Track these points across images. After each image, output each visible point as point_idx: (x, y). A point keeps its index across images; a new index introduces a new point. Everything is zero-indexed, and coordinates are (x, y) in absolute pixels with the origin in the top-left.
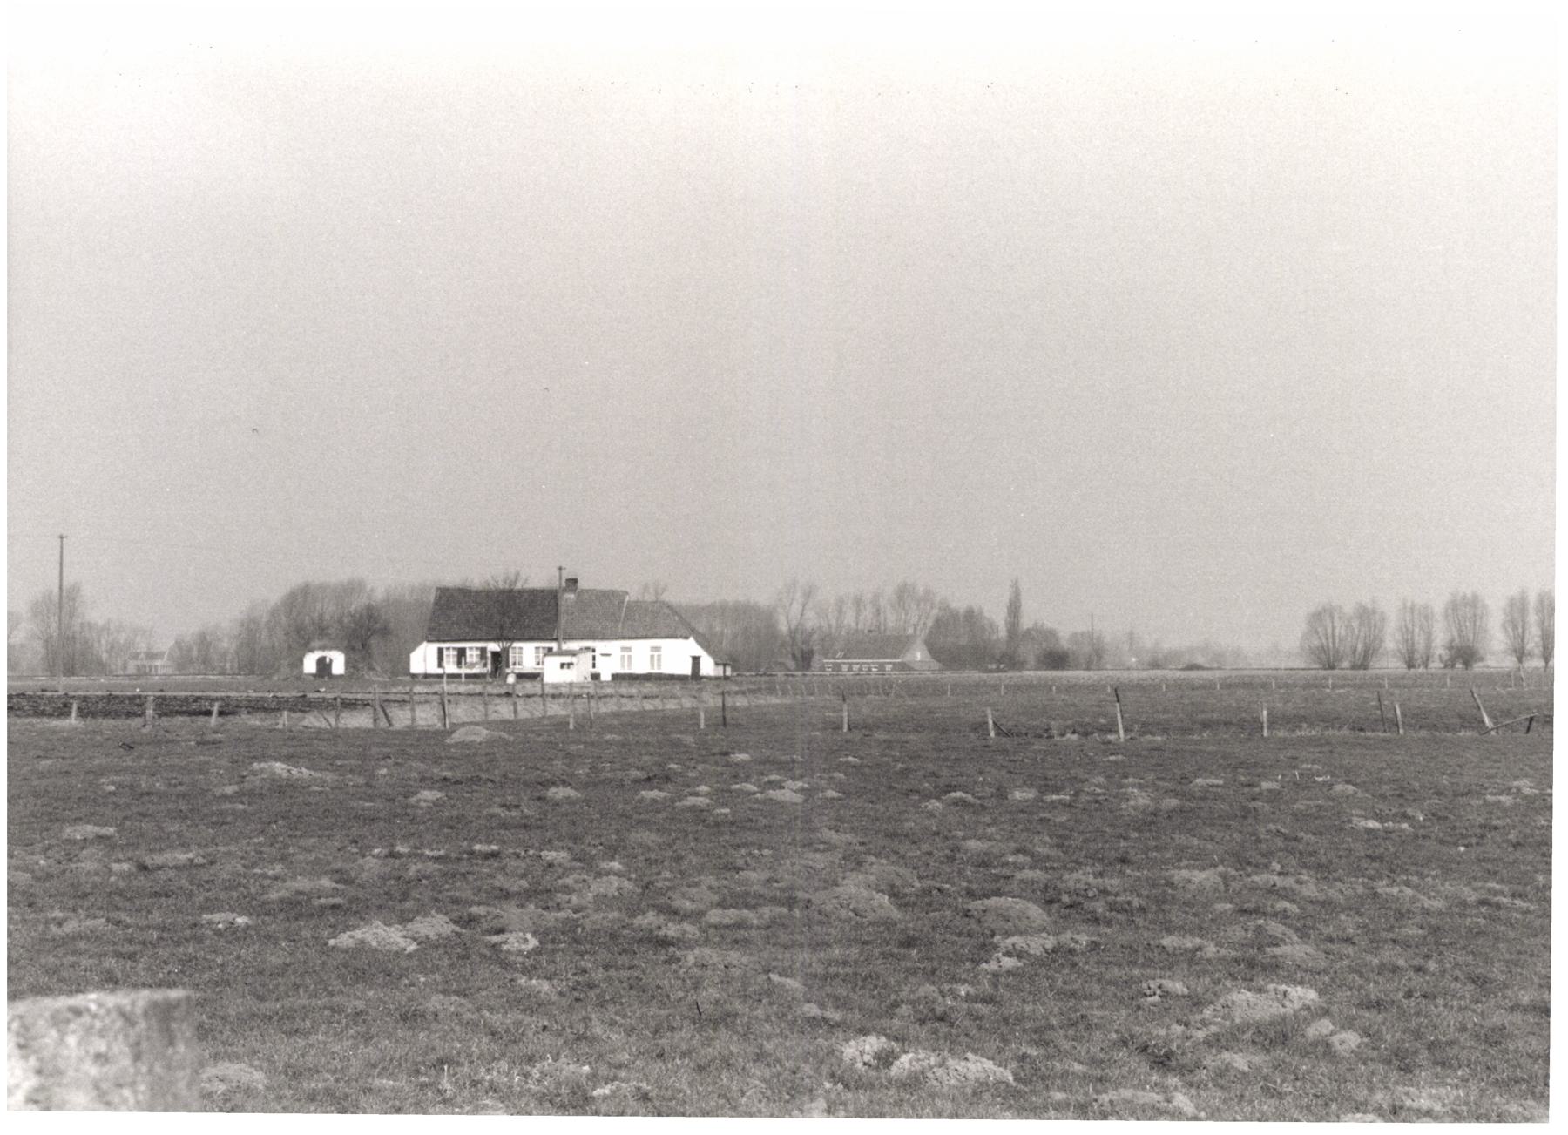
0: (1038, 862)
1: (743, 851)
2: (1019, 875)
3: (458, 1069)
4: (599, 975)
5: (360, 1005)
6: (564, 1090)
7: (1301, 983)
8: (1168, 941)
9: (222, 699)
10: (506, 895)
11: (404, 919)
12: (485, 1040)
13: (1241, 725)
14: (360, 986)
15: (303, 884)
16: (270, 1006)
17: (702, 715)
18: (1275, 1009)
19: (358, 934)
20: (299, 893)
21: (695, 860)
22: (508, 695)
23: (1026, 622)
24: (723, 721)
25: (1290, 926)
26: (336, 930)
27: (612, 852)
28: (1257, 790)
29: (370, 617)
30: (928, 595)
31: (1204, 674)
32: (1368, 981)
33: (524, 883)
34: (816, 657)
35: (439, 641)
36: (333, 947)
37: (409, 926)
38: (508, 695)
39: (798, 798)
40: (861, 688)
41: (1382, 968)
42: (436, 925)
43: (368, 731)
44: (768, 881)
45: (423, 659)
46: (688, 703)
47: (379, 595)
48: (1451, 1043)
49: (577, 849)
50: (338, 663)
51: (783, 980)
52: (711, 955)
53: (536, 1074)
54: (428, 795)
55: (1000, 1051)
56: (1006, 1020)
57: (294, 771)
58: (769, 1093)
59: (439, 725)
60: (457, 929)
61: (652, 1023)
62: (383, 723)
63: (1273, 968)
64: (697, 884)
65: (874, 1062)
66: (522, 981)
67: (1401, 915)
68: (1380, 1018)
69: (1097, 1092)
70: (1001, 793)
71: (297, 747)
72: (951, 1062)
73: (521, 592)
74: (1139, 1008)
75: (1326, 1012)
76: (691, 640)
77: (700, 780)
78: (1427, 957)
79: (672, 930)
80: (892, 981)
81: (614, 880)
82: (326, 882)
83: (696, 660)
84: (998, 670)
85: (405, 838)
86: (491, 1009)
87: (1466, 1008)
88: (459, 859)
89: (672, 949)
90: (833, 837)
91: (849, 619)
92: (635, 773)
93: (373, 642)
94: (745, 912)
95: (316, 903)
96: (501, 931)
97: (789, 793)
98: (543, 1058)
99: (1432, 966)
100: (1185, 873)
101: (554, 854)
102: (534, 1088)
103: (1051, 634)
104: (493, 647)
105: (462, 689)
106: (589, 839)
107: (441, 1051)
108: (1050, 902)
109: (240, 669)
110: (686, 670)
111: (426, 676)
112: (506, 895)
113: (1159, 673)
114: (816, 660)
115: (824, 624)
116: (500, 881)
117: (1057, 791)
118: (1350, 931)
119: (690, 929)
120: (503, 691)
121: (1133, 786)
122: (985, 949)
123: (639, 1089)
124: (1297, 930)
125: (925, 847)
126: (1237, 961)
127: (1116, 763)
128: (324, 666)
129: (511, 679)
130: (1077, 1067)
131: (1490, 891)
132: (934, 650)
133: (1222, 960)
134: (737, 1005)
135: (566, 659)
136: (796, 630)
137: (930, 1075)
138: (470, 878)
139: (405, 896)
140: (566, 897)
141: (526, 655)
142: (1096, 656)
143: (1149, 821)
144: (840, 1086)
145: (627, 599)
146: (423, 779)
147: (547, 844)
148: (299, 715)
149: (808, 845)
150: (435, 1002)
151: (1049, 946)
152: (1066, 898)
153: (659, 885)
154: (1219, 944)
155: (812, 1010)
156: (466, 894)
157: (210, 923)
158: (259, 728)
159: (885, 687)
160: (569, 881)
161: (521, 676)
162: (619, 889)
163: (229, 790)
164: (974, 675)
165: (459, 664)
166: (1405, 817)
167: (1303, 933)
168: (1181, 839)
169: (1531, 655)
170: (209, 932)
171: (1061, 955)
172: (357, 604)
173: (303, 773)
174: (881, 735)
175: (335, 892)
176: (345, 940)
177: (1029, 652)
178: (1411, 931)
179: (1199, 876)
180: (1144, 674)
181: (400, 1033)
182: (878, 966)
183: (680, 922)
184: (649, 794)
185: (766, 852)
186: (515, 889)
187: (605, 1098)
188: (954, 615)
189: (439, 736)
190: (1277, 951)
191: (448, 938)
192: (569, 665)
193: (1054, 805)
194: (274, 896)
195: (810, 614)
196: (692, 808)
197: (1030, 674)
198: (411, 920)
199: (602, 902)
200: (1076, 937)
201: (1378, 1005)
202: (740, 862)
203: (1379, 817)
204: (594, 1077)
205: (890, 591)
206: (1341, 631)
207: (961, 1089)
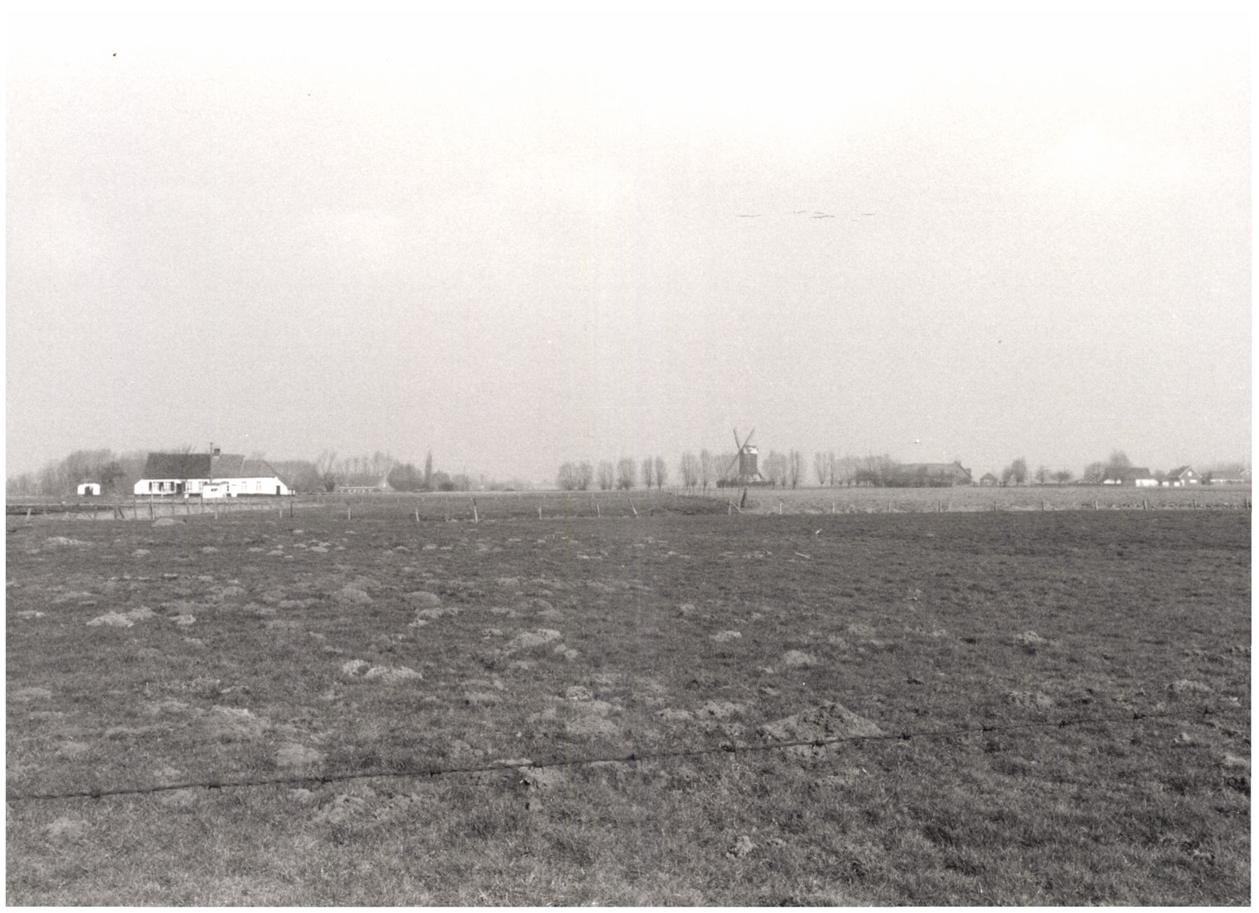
0: (436, 575)
1: (298, 574)
2: (428, 582)
3: (154, 684)
4: (226, 635)
5: (103, 655)
6: (207, 691)
7: (553, 628)
8: (495, 610)
9: (33, 507)
10: (179, 597)
11: (127, 610)
12: (168, 670)
13: (530, 515)
14: (103, 646)
15: (74, 594)
16: (53, 659)
17: (281, 513)
18: (541, 641)
19: (102, 618)
20: (71, 599)
21: (275, 578)
22: (184, 504)
23: (435, 470)
24: (291, 515)
25: (549, 601)
26: (90, 616)
27: (234, 576)
28: (535, 543)
29: (113, 468)
30: (389, 459)
31: (514, 493)
32: (582, 626)
33: (189, 591)
34: (336, 486)
35: (149, 478)
36: (90, 626)
37: (130, 613)
38: (184, 504)
39: (326, 550)
40: (358, 499)
41: (588, 620)
42: (144, 613)
43: (111, 521)
44: (310, 587)
45: (141, 487)
46: (274, 507)
47: (118, 457)
48: (617, 653)
49: (217, 575)
50: (96, 489)
51: (315, 635)
52: (280, 623)
53: (194, 685)
54: (142, 552)
55: (417, 665)
56: (420, 650)
57: (71, 541)
58: (308, 688)
59: (149, 518)
60: (155, 614)
61: (252, 658)
62: (119, 517)
63: (540, 621)
64: (276, 589)
65: (358, 673)
66: (188, 640)
67: (598, 595)
68: (586, 643)
69: (461, 681)
70: (421, 546)
71: (71, 529)
72: (394, 671)
73: (191, 456)
74: (480, 642)
75: (563, 641)
76: (276, 478)
77: (279, 543)
78: (607, 614)
79: (263, 611)
80: (367, 634)
81: (235, 587)
82: (86, 594)
83: (278, 488)
84: (421, 492)
85: (130, 572)
86: (172, 654)
87: (623, 637)
88: (156, 581)
89: (262, 621)
90: (342, 567)
91: (352, 469)
92: (247, 540)
93: (115, 480)
94: (298, 602)
95: (80, 603)
96: (177, 614)
97: (321, 548)
98: (196, 677)
99: (609, 618)
100: (503, 579)
101: (205, 577)
102: (191, 690)
103: (446, 476)
104: (177, 481)
105: (161, 501)
106: (223, 570)
107: (145, 675)
108: (442, 593)
109: (43, 492)
110: (274, 492)
111: (143, 495)
112: (179, 597)
113: (494, 493)
114: (337, 487)
115: (340, 471)
116: (177, 590)
117: (445, 545)
118: (574, 603)
119: (272, 611)
120: (181, 502)
121: (481, 542)
122: (411, 616)
123: (244, 689)
124: (552, 603)
125: (385, 570)
126: (525, 619)
127: (473, 532)
128: (88, 491)
129: (187, 496)
130: (452, 671)
131: (634, 583)
132: (391, 482)
133: (518, 618)
134: (293, 647)
135: (214, 487)
136: (327, 474)
137: (384, 677)
138: (163, 589)
139: (128, 599)
140: (210, 597)
141: (194, 485)
142: (466, 484)
143: (488, 558)
144: (341, 684)
145: (245, 459)
146: (139, 544)
147: (202, 573)
148: (74, 514)
149: (330, 571)
150: (141, 653)
151: (440, 614)
152: (449, 592)
153: (258, 589)
154: (517, 611)
155: (329, 648)
156: (161, 597)
157: (21, 616)
158: (53, 521)
159: (368, 499)
160: (212, 589)
161: (191, 495)
162: (237, 592)
163: (35, 551)
164: (409, 494)
165: (160, 489)
166: (599, 554)
167: (555, 606)
168: (501, 565)
169: (653, 483)
170: (21, 621)
171: (446, 617)
172: (105, 462)
173: (75, 542)
174: (366, 521)
175: (90, 598)
176: (95, 622)
177: (435, 484)
178: (601, 602)
179: (508, 580)
180: (487, 493)
181: (124, 669)
182: (362, 627)
183: (267, 607)
184: (253, 550)
185: (310, 574)
186: (184, 594)
187: (228, 694)
188: (401, 467)
189: (148, 523)
190: (542, 613)
191: (150, 619)
192: (216, 490)
193: (444, 552)
194: (58, 601)
195: (333, 466)
196: (274, 556)
197: (436, 493)
198: (131, 610)
199: (228, 598)
200: (453, 609)
201: (586, 637)
202: (296, 579)
203: (588, 554)
204: (222, 684)
205: (371, 457)
206: (573, 474)
207: (398, 682)
